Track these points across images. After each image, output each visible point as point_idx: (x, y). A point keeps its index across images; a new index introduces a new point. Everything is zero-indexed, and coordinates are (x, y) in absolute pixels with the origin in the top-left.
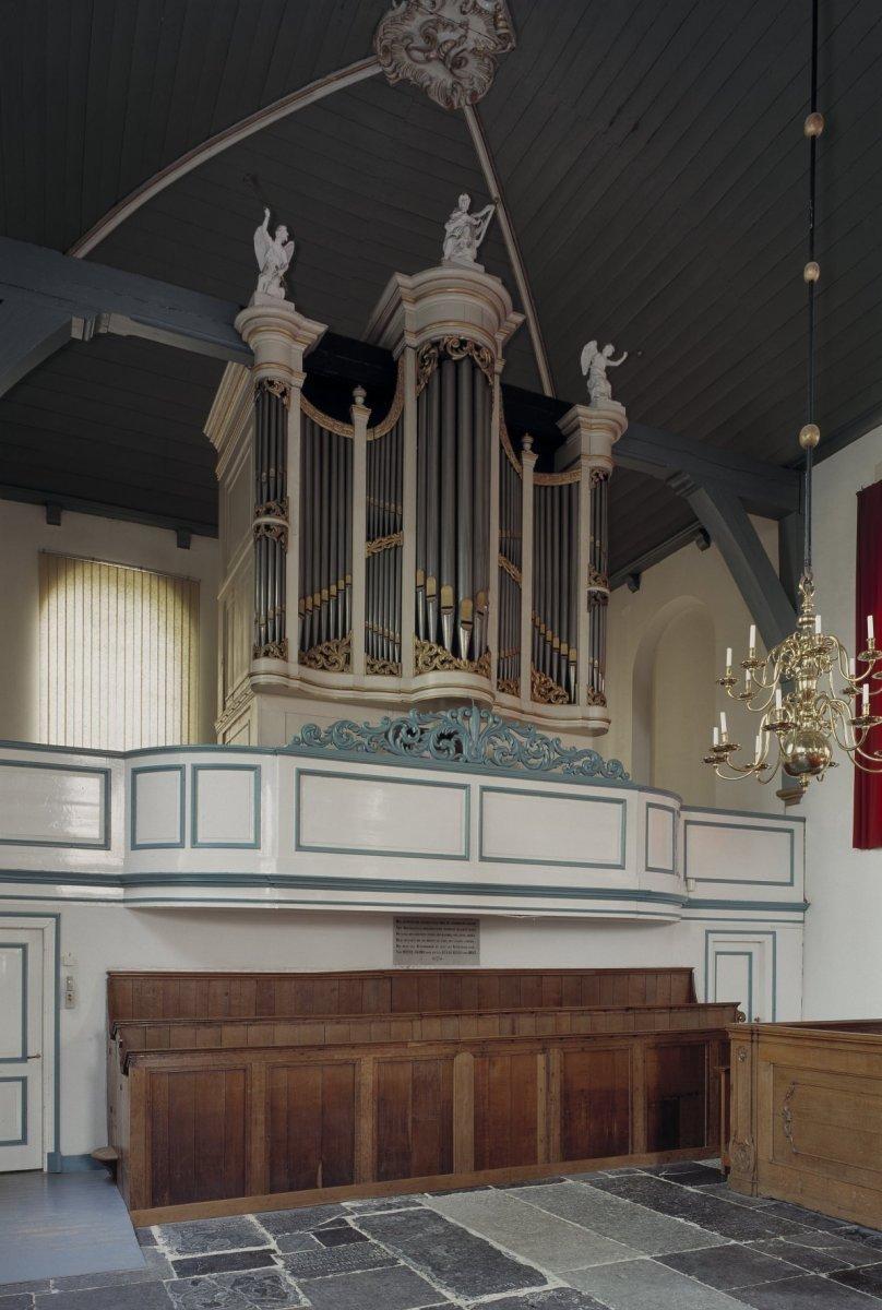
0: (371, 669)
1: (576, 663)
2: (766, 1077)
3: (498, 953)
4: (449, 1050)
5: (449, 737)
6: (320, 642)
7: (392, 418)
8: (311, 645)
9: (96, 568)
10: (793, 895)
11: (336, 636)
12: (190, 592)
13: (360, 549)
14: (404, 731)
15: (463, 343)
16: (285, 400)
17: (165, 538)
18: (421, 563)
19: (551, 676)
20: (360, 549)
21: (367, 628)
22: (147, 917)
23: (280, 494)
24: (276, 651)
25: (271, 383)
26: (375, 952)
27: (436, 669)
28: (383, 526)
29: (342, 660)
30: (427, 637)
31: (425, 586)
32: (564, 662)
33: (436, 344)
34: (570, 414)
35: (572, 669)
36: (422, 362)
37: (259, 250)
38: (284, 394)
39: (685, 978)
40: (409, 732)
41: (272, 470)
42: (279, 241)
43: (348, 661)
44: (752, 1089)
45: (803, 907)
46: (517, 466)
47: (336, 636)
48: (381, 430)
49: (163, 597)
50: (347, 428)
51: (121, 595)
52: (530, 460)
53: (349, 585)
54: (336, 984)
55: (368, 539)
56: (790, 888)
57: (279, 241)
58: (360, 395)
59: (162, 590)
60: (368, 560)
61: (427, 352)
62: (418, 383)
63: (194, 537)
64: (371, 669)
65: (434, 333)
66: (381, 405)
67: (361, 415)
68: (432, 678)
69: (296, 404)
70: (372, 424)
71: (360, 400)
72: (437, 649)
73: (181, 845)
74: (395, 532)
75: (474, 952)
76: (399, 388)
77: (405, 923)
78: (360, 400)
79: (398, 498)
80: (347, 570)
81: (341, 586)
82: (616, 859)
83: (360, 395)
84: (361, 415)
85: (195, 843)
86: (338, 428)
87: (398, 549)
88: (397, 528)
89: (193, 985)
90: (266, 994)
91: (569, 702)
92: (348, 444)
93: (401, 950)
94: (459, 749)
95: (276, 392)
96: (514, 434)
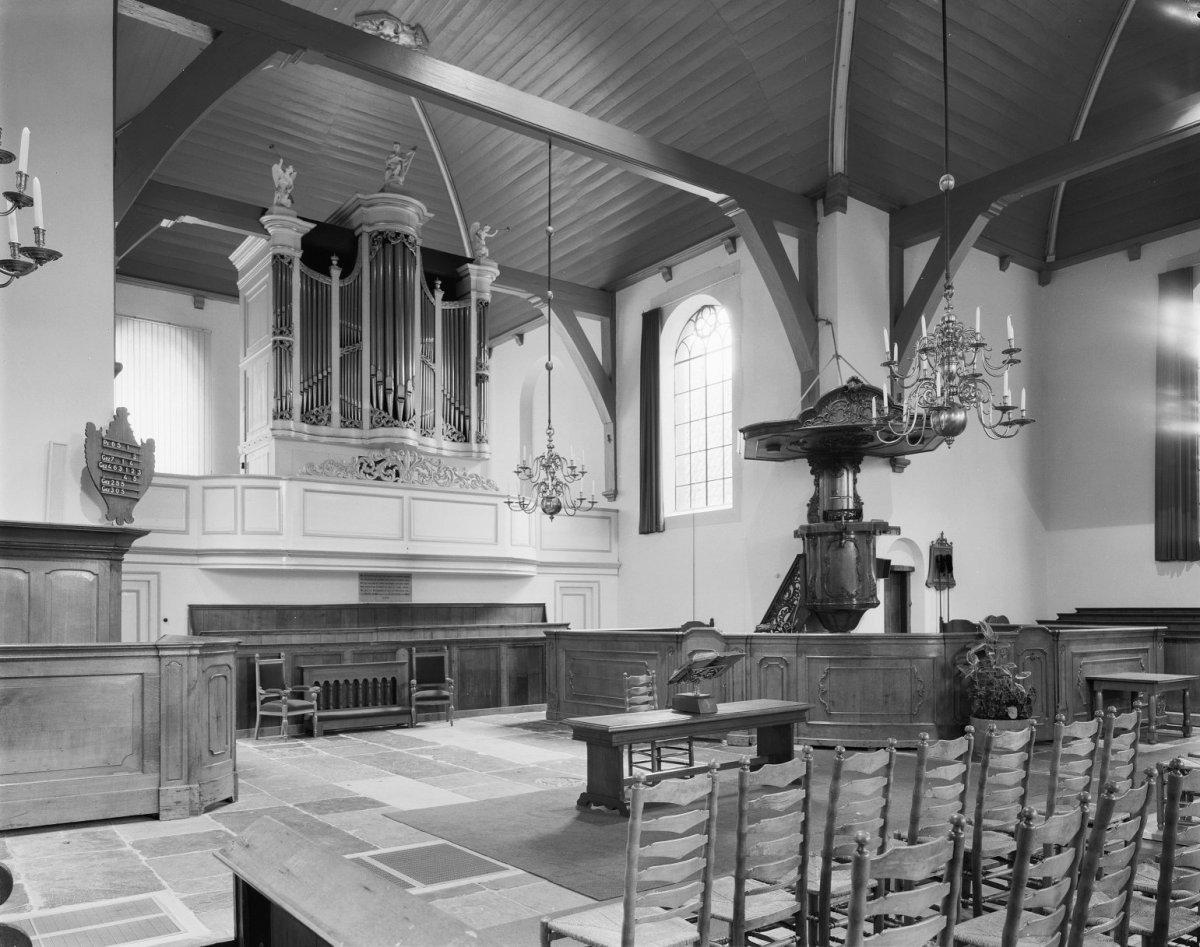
0: (344, 425)
1: (469, 417)
2: (562, 657)
3: (424, 594)
4: (393, 647)
5: (392, 468)
6: (312, 408)
7: (355, 273)
8: (307, 410)
9: (136, 325)
10: (611, 559)
11: (322, 404)
12: (201, 337)
13: (336, 352)
14: (365, 465)
15: (398, 234)
16: (291, 266)
17: (182, 300)
18: (373, 362)
19: (455, 425)
20: (336, 352)
21: (341, 400)
22: (215, 575)
23: (289, 324)
24: (288, 416)
25: (282, 257)
26: (347, 594)
27: (383, 426)
28: (350, 340)
29: (326, 419)
30: (378, 406)
31: (376, 375)
32: (462, 417)
33: (381, 233)
34: (464, 267)
35: (467, 421)
36: (373, 242)
37: (275, 177)
38: (290, 263)
39: (541, 609)
40: (368, 466)
41: (284, 308)
42: (288, 173)
43: (329, 420)
44: (558, 661)
45: (619, 567)
46: (432, 300)
47: (322, 404)
48: (348, 281)
49: (184, 345)
50: (327, 279)
51: (137, 339)
52: (439, 294)
53: (329, 373)
54: (324, 612)
55: (341, 346)
56: (608, 554)
57: (288, 173)
58: (335, 260)
59: (184, 339)
60: (341, 358)
61: (376, 237)
62: (371, 254)
63: (206, 300)
64: (344, 425)
65: (381, 227)
66: (348, 266)
67: (336, 272)
68: (381, 431)
69: (297, 268)
70: (342, 277)
71: (335, 262)
72: (384, 414)
73: (235, 533)
74: (358, 342)
75: (408, 594)
76: (358, 259)
77: (365, 577)
78: (335, 262)
79: (359, 321)
80: (329, 365)
81: (325, 374)
82: (247, 491)
83: (335, 260)
84: (336, 272)
85: (244, 532)
86: (322, 279)
87: (359, 353)
88: (359, 340)
89: (239, 612)
90: (283, 616)
91: (466, 441)
92: (328, 288)
93: (363, 592)
94: (398, 475)
95: (285, 262)
96: (429, 280)
